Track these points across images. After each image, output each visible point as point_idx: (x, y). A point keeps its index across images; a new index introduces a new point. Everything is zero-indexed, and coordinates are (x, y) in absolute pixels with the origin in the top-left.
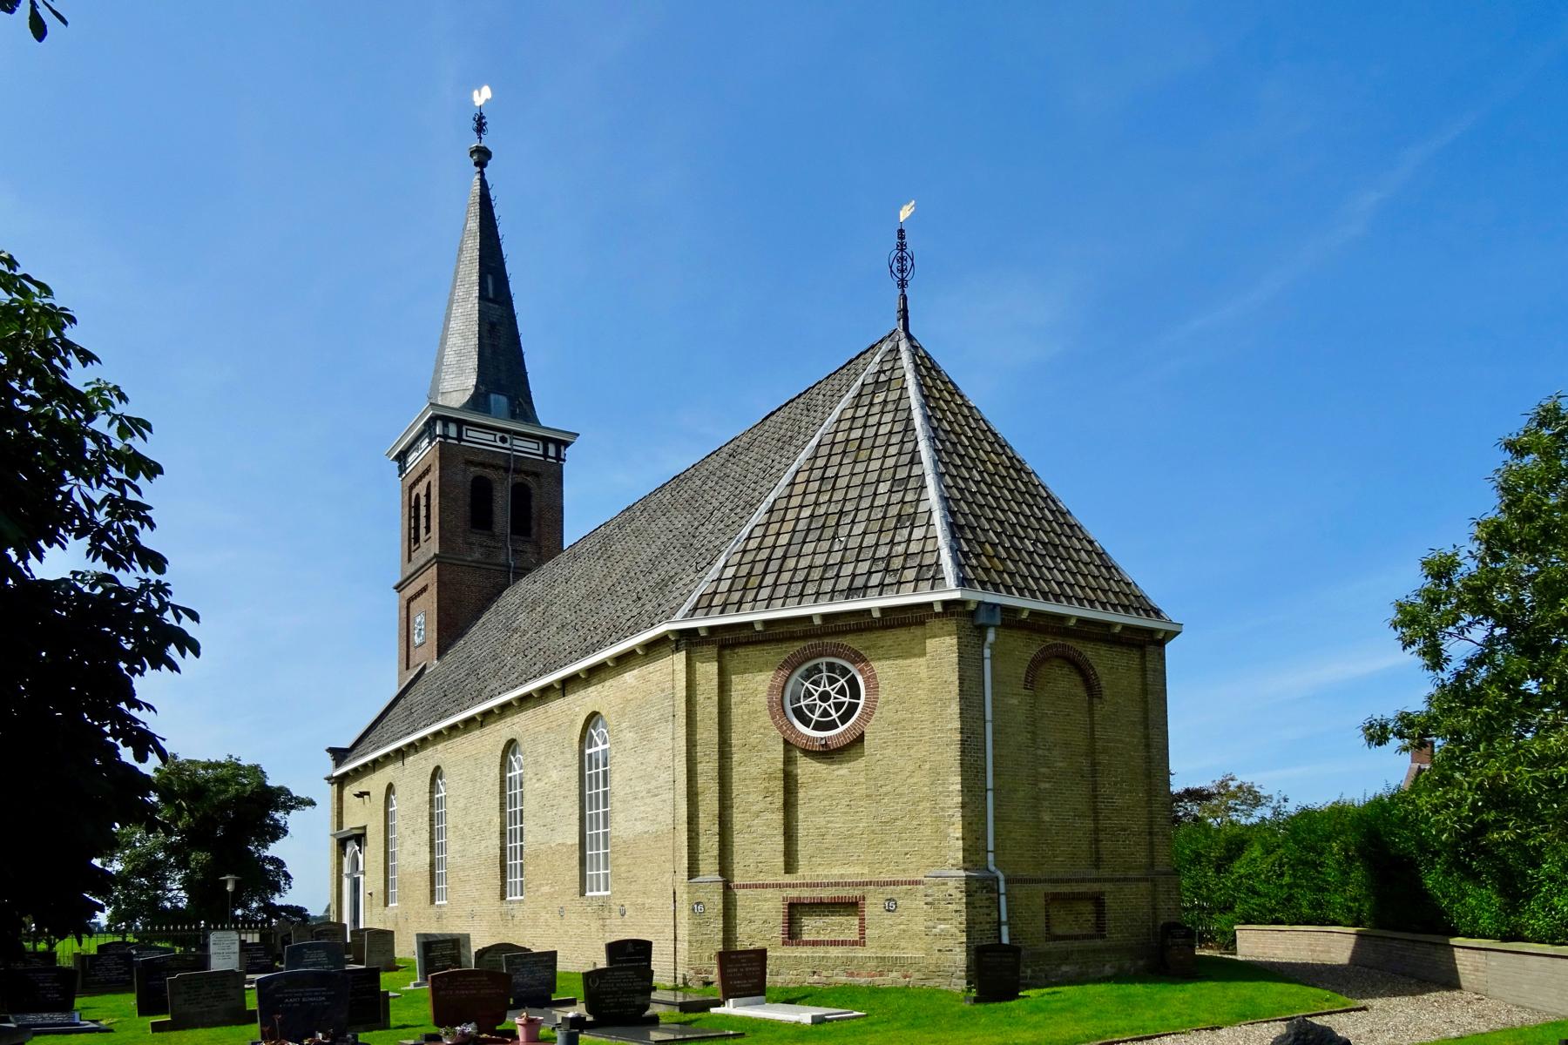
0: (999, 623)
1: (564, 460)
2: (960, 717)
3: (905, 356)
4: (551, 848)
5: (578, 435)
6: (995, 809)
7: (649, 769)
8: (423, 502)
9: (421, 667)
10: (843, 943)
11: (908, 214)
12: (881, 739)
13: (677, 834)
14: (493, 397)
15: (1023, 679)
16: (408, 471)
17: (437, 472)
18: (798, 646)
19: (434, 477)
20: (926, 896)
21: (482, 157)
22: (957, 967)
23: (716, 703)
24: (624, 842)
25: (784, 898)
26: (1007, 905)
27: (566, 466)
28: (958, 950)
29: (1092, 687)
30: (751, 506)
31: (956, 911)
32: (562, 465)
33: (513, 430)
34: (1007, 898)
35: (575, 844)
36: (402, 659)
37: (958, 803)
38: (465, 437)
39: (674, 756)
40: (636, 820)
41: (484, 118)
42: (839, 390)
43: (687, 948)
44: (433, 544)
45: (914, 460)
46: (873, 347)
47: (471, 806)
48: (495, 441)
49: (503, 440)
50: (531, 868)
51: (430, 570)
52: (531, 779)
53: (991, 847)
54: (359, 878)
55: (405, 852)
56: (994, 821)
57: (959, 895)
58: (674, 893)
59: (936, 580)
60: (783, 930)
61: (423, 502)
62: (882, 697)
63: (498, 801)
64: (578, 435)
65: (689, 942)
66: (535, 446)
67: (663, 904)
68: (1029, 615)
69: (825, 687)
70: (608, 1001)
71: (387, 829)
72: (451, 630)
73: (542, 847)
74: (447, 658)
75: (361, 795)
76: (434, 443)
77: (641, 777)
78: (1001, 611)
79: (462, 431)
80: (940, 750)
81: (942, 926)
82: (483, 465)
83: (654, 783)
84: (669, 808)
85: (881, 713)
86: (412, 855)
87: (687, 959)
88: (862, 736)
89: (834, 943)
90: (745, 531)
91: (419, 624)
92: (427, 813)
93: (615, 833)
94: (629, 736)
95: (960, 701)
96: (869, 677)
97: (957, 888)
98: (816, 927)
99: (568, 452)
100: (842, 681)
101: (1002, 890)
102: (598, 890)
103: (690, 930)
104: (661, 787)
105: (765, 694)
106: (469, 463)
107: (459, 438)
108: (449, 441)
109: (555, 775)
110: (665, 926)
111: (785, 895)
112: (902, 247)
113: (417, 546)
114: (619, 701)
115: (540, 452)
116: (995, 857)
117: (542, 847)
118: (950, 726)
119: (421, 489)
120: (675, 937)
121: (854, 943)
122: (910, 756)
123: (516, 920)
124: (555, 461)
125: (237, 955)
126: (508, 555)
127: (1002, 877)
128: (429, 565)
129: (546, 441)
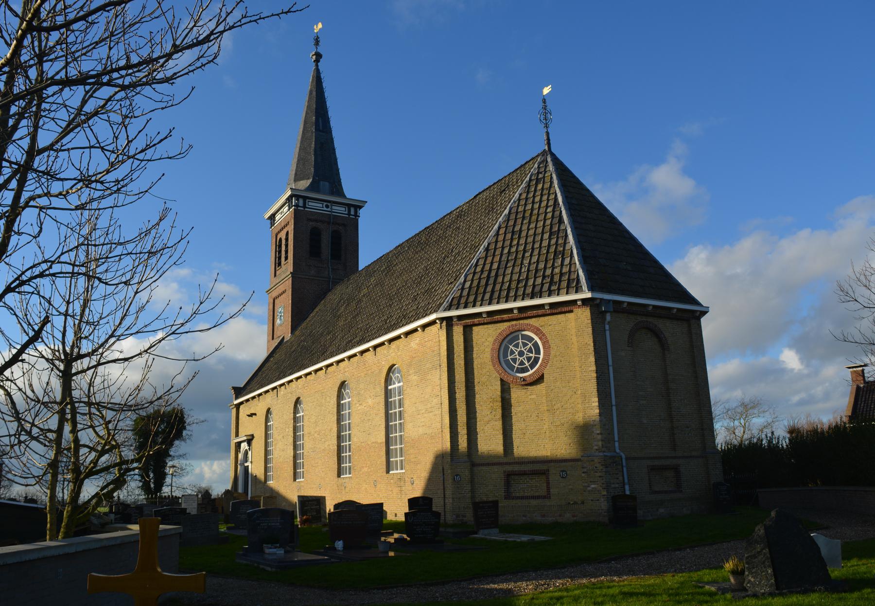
0: (612, 310)
1: (359, 216)
2: (595, 364)
3: (551, 167)
4: (368, 445)
5: (366, 202)
6: (617, 416)
7: (426, 397)
8: (284, 242)
9: (281, 338)
10: (538, 497)
11: (548, 91)
12: (553, 377)
13: (444, 435)
14: (322, 183)
15: (627, 341)
16: (275, 225)
17: (293, 226)
18: (506, 324)
19: (291, 228)
20: (583, 468)
21: (318, 56)
22: (602, 510)
23: (463, 358)
24: (413, 440)
25: (504, 471)
26: (628, 473)
27: (360, 220)
28: (602, 499)
29: (663, 344)
30: (476, 247)
31: (600, 477)
32: (358, 219)
33: (332, 201)
34: (627, 469)
35: (383, 442)
36: (270, 334)
37: (597, 413)
38: (307, 206)
39: (441, 389)
40: (419, 427)
41: (319, 38)
42: (517, 182)
43: (451, 501)
44: (289, 267)
45: (561, 221)
46: (533, 159)
47: (319, 421)
48: (323, 207)
49: (327, 206)
50: (356, 458)
51: (287, 282)
52: (356, 404)
53: (616, 439)
54: (248, 466)
55: (278, 449)
56: (617, 423)
57: (601, 468)
58: (443, 469)
59: (578, 290)
60: (505, 491)
61: (284, 242)
62: (553, 352)
63: (336, 417)
64: (366, 202)
65: (453, 498)
66: (344, 209)
67: (436, 476)
68: (627, 305)
69: (521, 348)
70: (417, 530)
71: (267, 436)
72: (298, 316)
73: (363, 444)
74: (297, 333)
75: (251, 415)
76: (291, 210)
77: (422, 402)
78: (613, 303)
79: (306, 202)
80: (586, 383)
81: (593, 486)
82: (316, 221)
83: (429, 405)
84: (438, 419)
85: (553, 362)
86: (282, 451)
87: (451, 509)
88: (543, 375)
89: (534, 497)
90: (474, 261)
91: (280, 313)
92: (292, 426)
93: (406, 435)
94: (414, 378)
95: (595, 355)
96: (544, 342)
97: (599, 463)
98: (523, 488)
99: (362, 212)
100: (520, 341)
101: (624, 464)
102: (397, 470)
103: (452, 491)
104: (434, 407)
105: (489, 353)
106: (309, 220)
107: (304, 206)
108: (299, 208)
109: (370, 401)
110: (438, 489)
111: (505, 470)
112: (545, 108)
113: (280, 267)
114: (408, 358)
115: (346, 213)
116: (619, 445)
117: (363, 444)
118: (590, 369)
119: (283, 235)
120: (444, 496)
121: (545, 497)
122: (569, 386)
123: (347, 490)
124: (354, 217)
125: (196, 509)
126: (329, 271)
127: (623, 456)
128: (287, 278)
129: (349, 206)
